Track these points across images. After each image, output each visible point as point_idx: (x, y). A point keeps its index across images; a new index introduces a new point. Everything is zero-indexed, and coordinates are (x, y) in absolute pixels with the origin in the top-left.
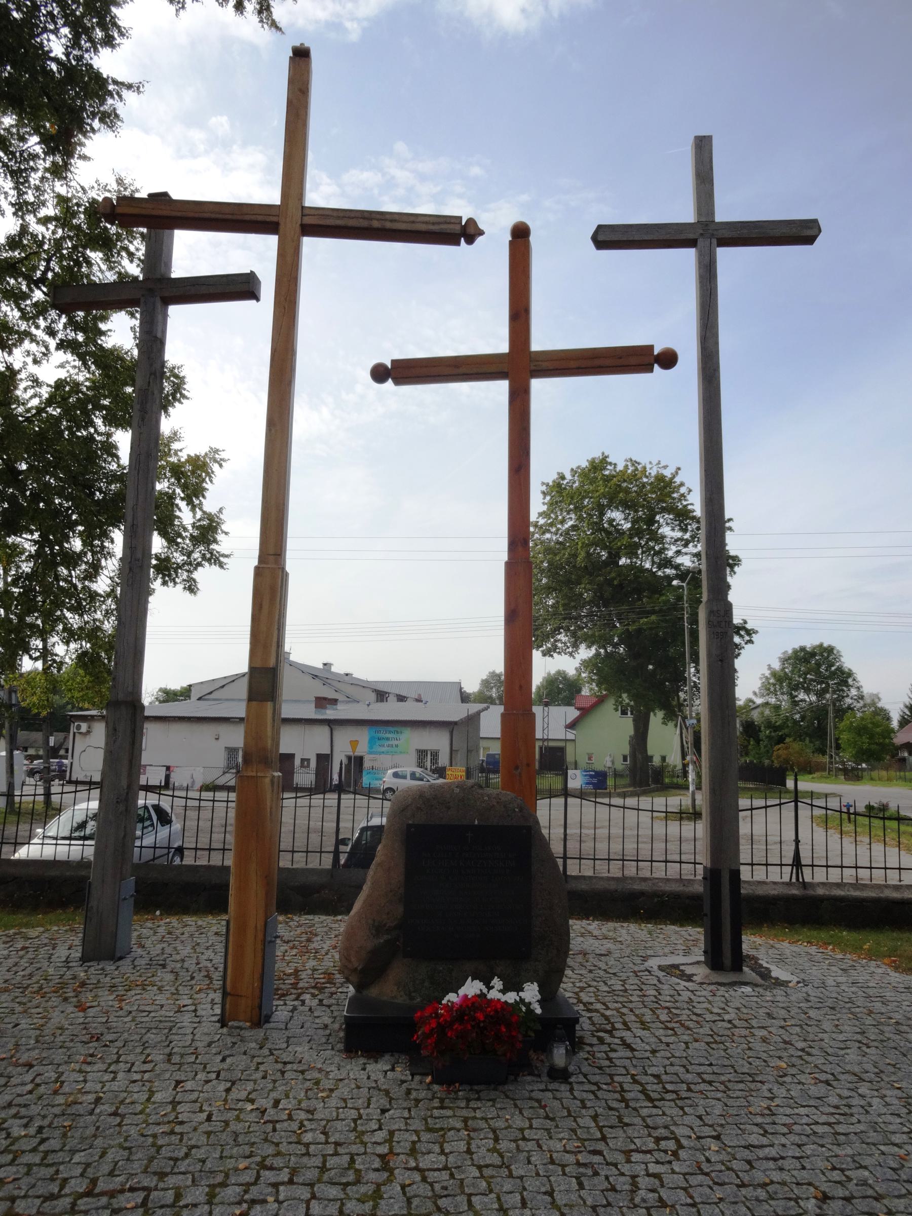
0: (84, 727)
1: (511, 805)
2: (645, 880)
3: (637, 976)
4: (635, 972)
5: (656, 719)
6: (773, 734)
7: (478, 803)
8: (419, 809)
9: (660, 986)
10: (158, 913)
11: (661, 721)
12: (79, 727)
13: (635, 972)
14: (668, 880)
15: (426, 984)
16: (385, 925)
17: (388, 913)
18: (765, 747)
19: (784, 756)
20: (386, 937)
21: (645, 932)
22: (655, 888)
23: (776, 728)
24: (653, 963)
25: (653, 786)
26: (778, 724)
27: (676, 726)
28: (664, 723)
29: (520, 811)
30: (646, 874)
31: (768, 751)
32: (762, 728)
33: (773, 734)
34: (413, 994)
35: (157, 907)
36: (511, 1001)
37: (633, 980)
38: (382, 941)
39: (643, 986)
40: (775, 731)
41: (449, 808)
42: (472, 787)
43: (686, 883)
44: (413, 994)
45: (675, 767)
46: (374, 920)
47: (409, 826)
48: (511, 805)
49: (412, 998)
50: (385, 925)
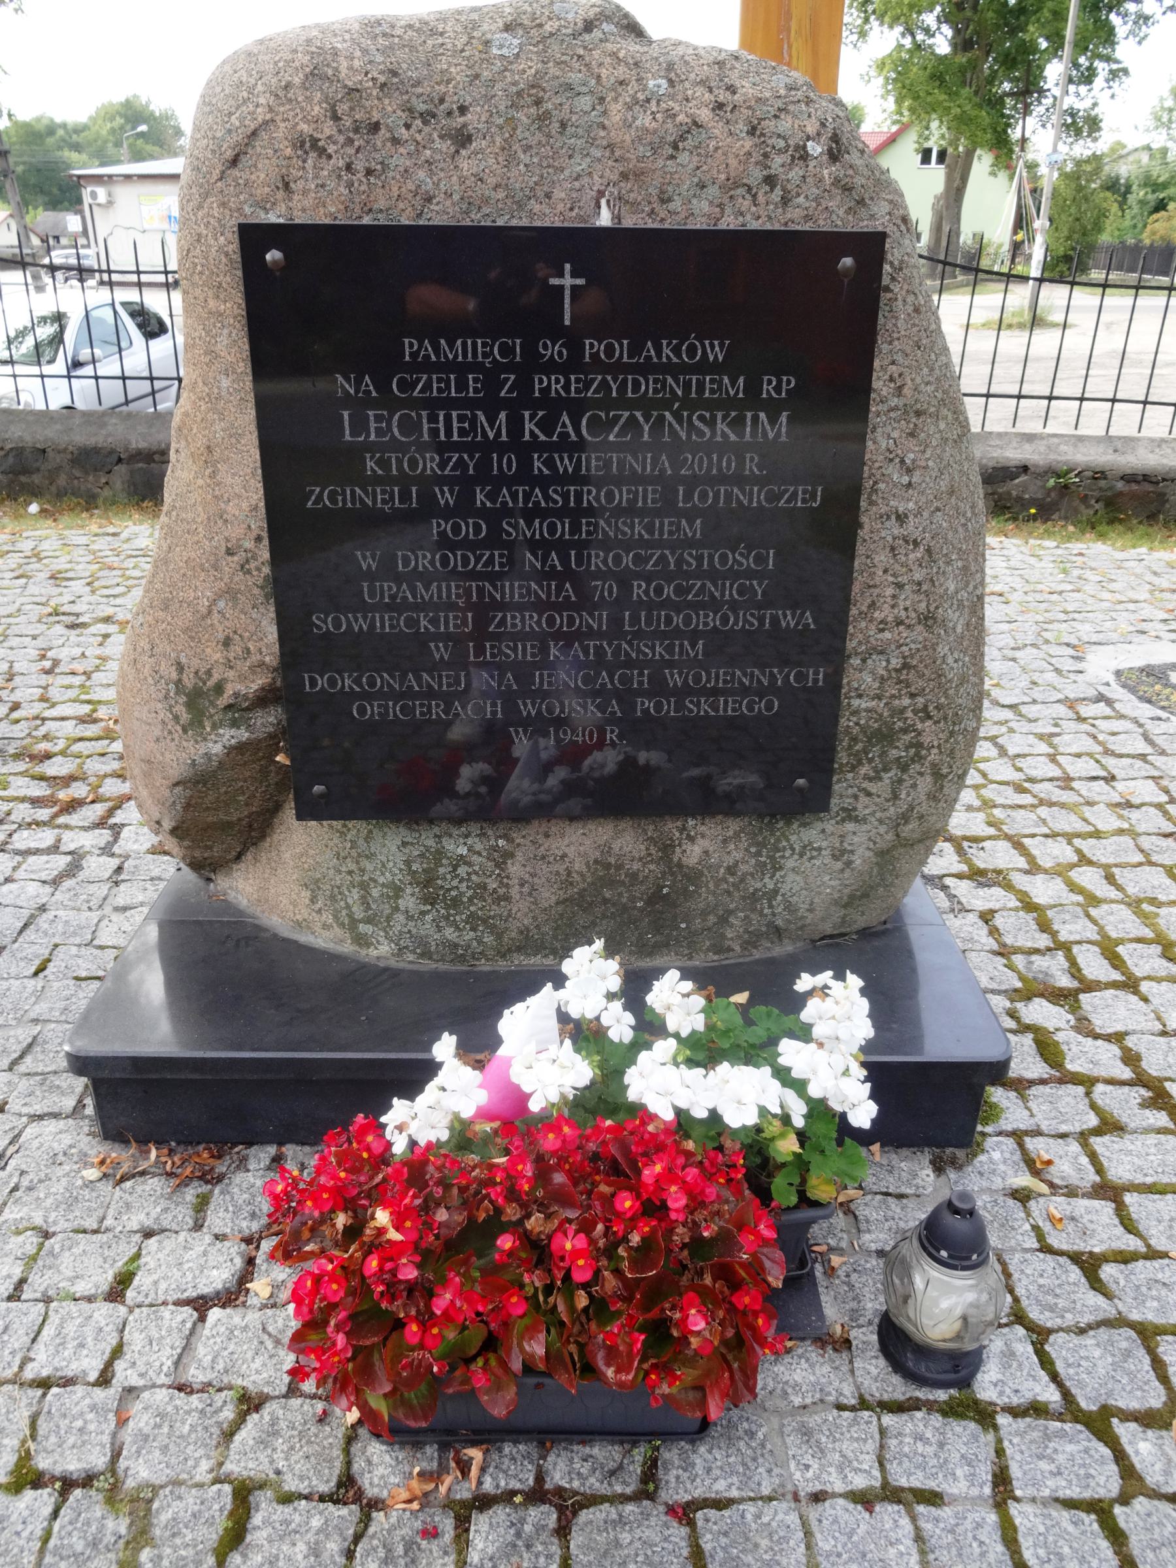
0: (101, 193)
1: (785, 124)
2: (1030, 438)
3: (1081, 719)
4: (1070, 703)
5: (982, 163)
6: (1150, 196)
7: (616, 112)
8: (310, 146)
9: (1159, 761)
10: (34, 508)
11: (989, 169)
12: (94, 195)
13: (1070, 703)
14: (1081, 439)
15: (409, 902)
16: (219, 689)
17: (227, 642)
18: (1133, 218)
19: (1162, 232)
20: (231, 736)
21: (1047, 564)
22: (1052, 457)
23: (1156, 187)
24: (1101, 666)
25: (960, 278)
26: (1161, 180)
27: (1011, 178)
28: (993, 174)
29: (834, 156)
30: (1032, 426)
31: (1135, 226)
32: (1134, 187)
33: (1150, 196)
34: (363, 928)
35: (35, 493)
36: (739, 1117)
37: (1073, 740)
38: (217, 749)
39: (1110, 762)
40: (1154, 192)
41: (462, 139)
42: (589, 26)
43: (1119, 445)
44: (363, 928)
45: (1000, 246)
46: (180, 668)
47: (254, 238)
48: (785, 124)
49: (361, 940)
50: (219, 689)
